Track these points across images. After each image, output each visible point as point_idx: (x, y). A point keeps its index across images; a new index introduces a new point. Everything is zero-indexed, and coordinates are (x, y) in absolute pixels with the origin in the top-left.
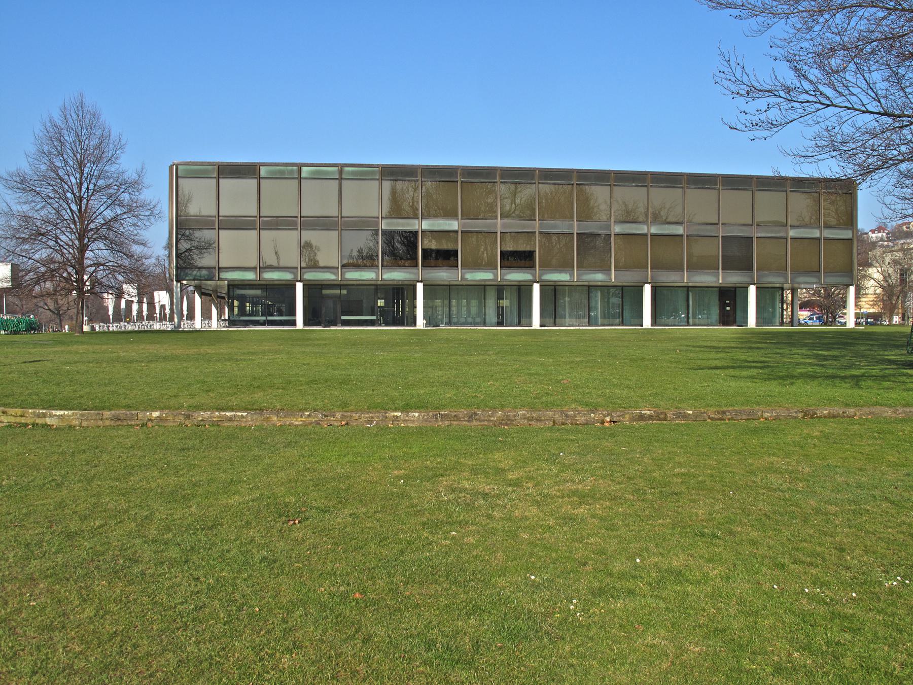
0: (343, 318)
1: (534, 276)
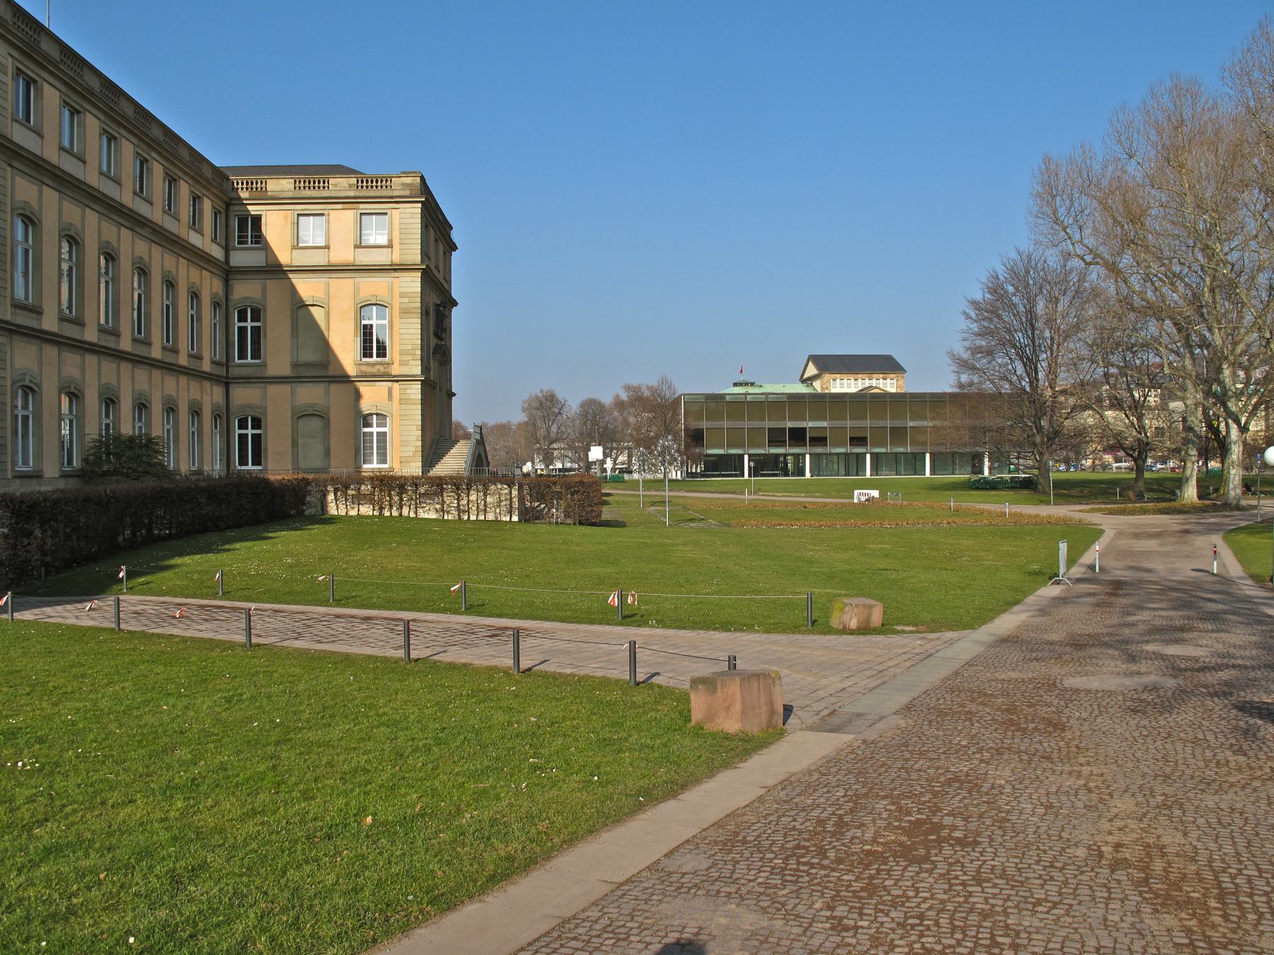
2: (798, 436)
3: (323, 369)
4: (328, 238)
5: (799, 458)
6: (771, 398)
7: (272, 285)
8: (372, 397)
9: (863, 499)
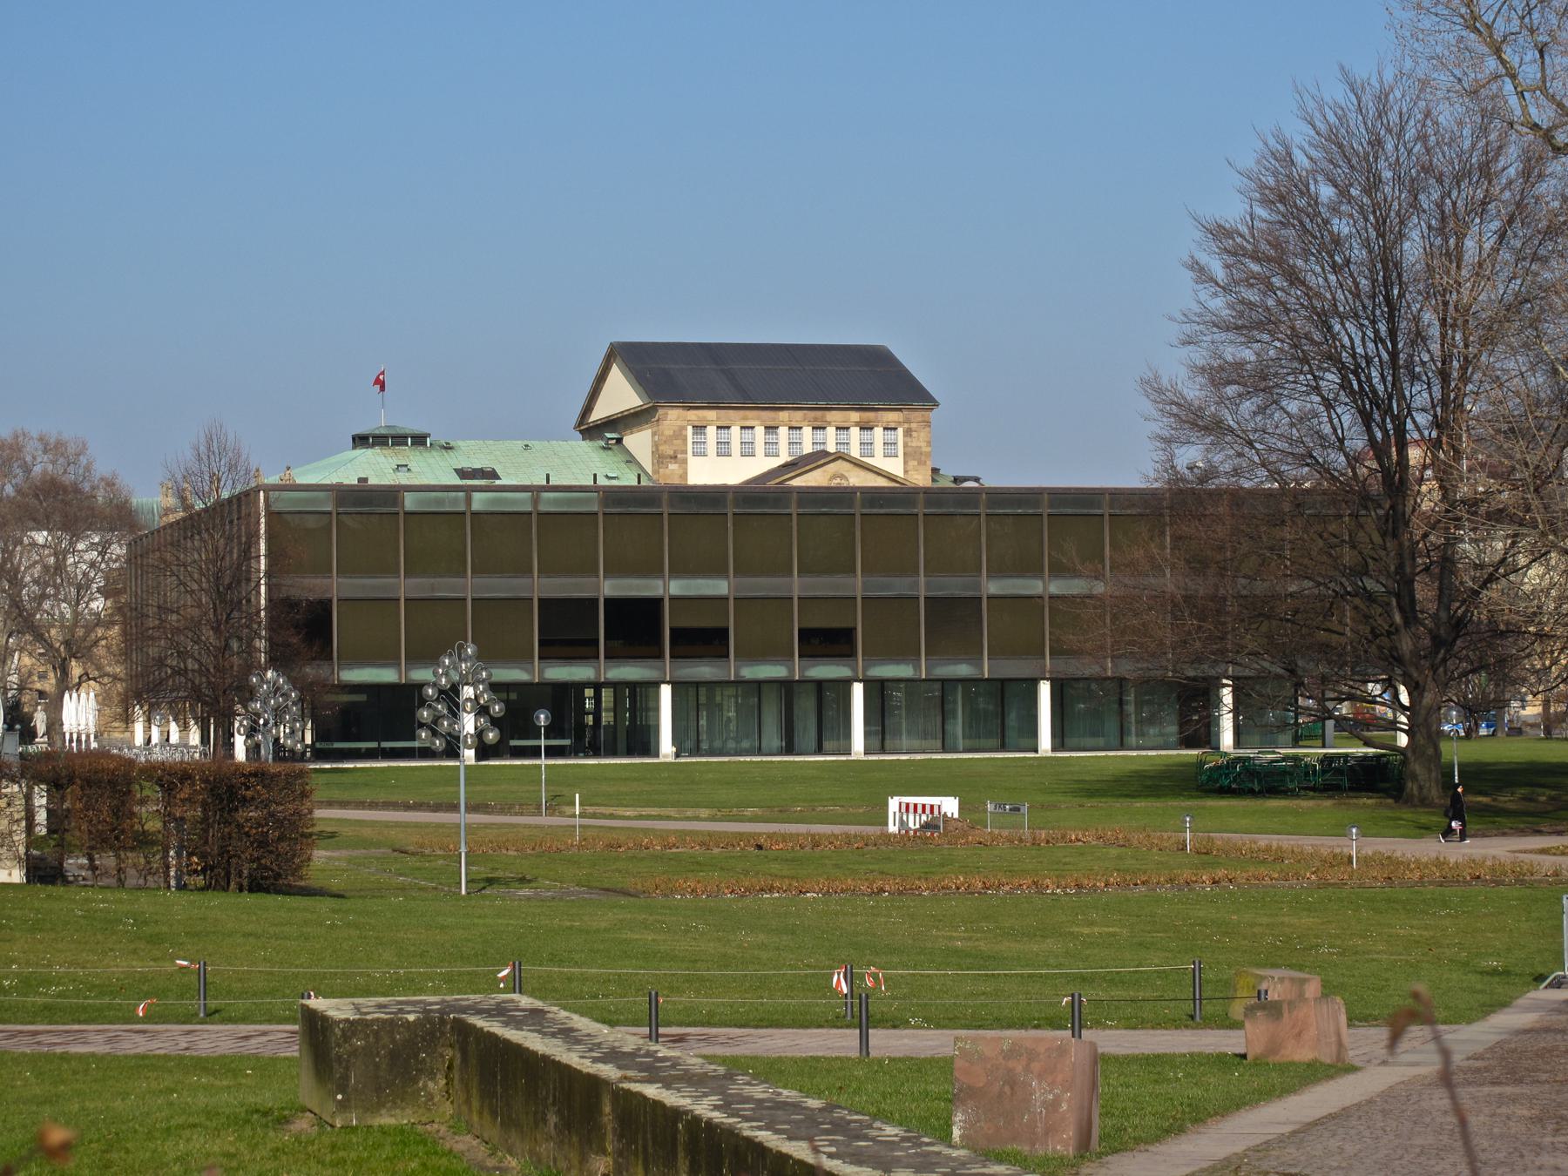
0: (513, 743)
1: (855, 670)
2: (635, 626)
5: (639, 697)
6: (549, 502)
9: (913, 822)
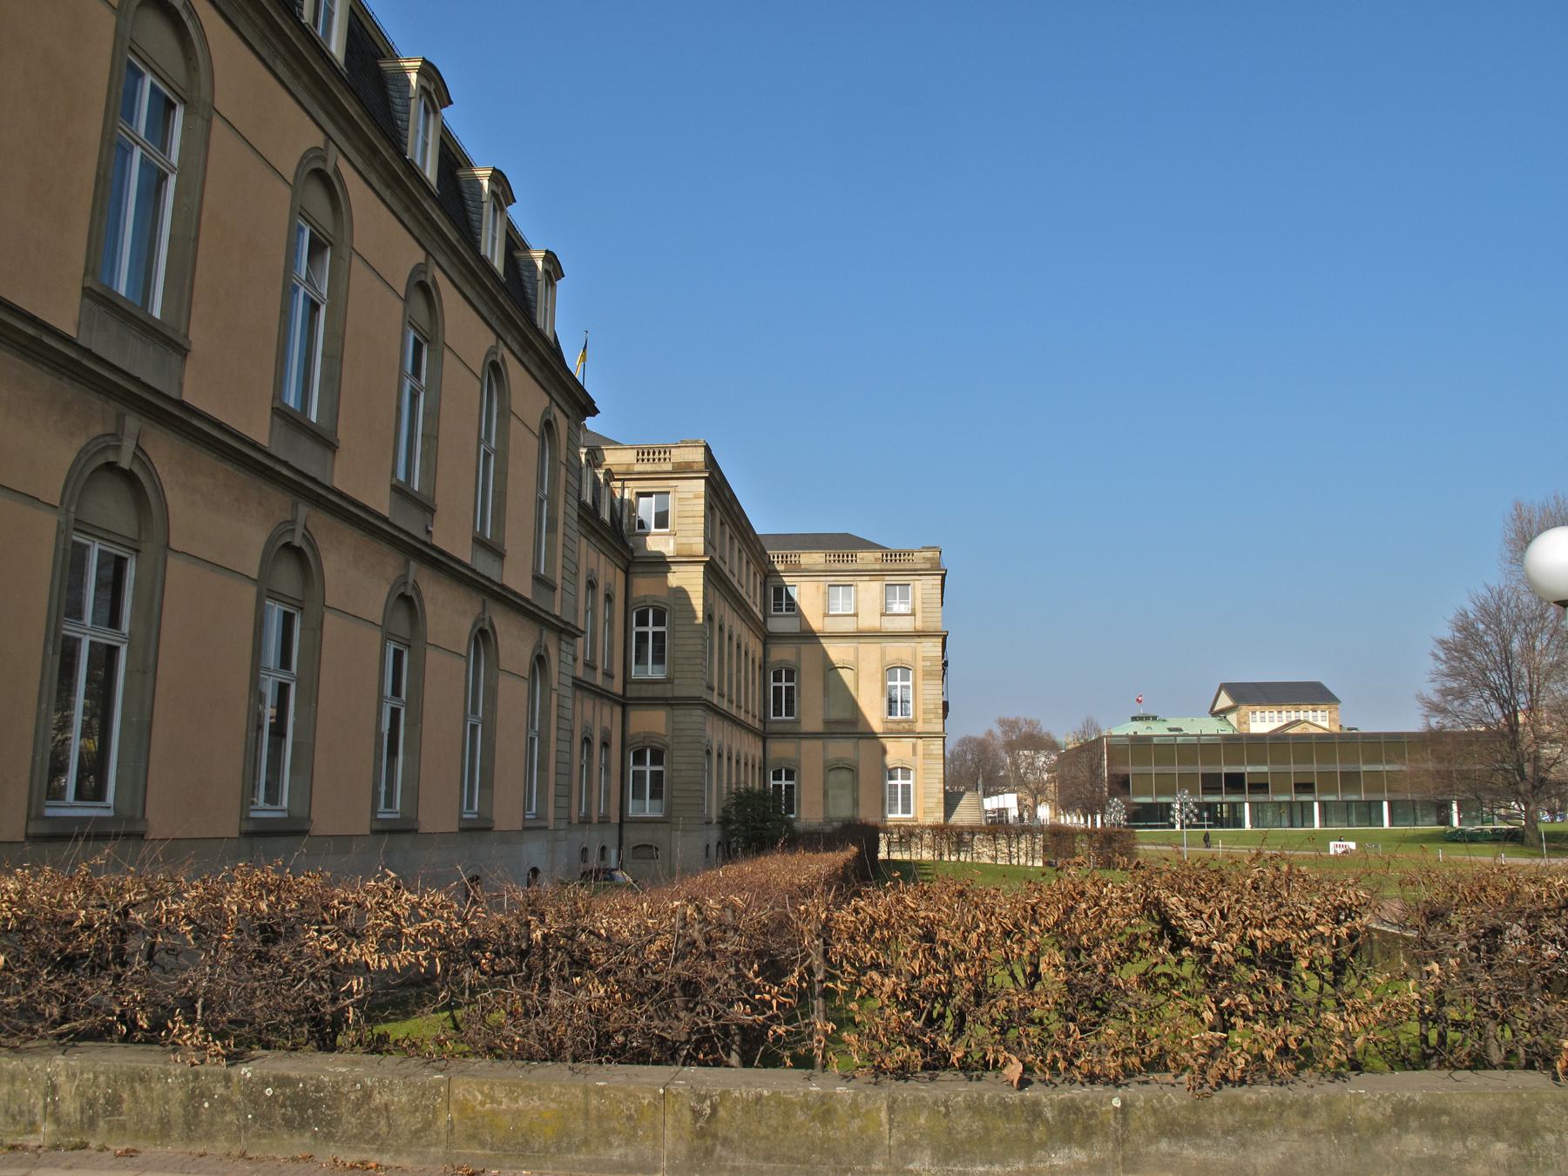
3: (850, 726)
4: (856, 607)
5: (1235, 808)
7: (806, 648)
8: (897, 751)
9: (1340, 851)
